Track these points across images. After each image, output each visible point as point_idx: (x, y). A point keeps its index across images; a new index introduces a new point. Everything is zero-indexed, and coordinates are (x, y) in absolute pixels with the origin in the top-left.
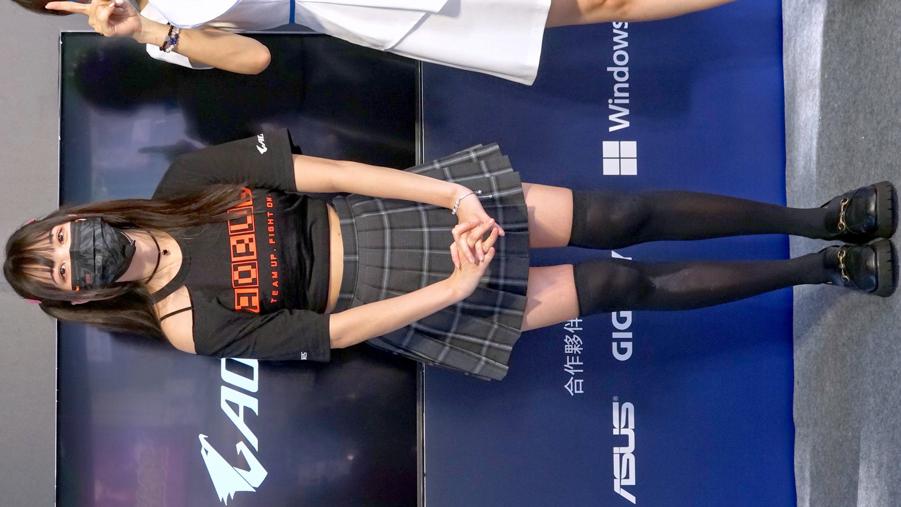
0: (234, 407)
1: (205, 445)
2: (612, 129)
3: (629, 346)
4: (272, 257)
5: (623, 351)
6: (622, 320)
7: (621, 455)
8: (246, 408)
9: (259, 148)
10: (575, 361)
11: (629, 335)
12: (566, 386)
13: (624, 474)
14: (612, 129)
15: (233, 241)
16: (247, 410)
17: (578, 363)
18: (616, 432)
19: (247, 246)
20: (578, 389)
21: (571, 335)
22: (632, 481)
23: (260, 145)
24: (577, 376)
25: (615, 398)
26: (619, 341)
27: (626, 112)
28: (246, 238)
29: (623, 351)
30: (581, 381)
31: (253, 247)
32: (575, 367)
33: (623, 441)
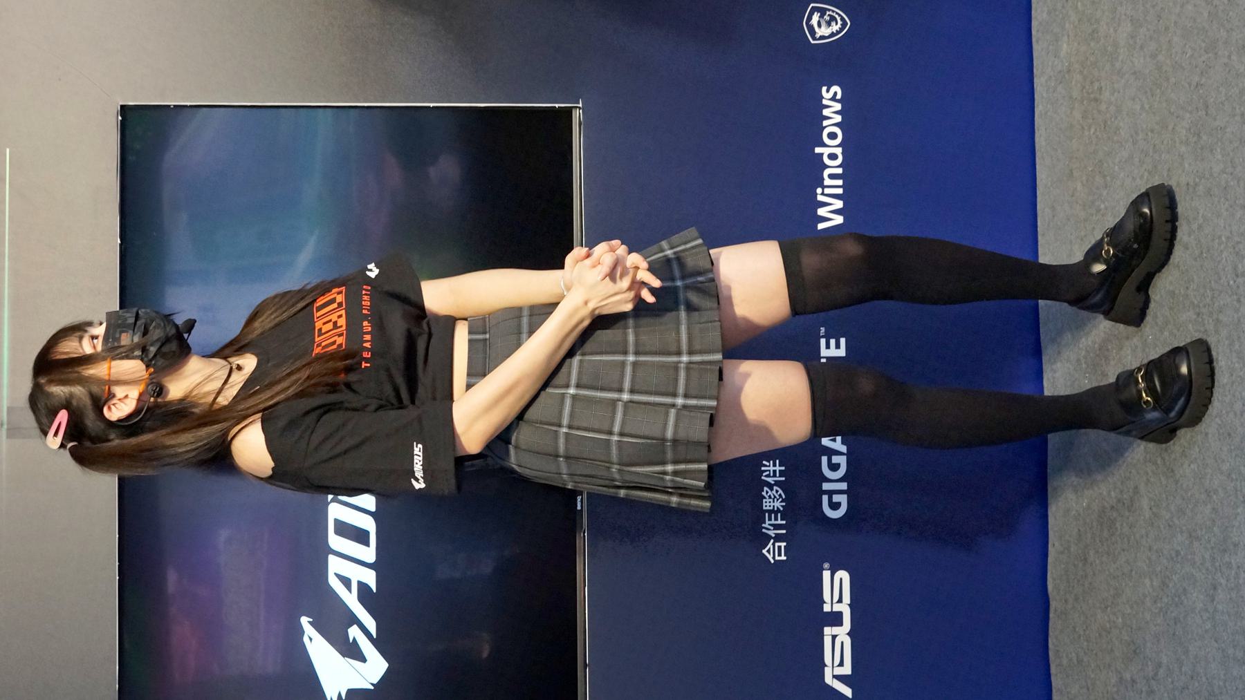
0: (346, 582)
1: (309, 630)
2: (821, 226)
3: (843, 499)
4: (365, 323)
5: (835, 506)
6: (834, 467)
7: (834, 637)
8: (360, 583)
9: (413, 482)
10: (776, 519)
11: (844, 486)
12: (764, 551)
13: (837, 661)
14: (821, 226)
15: (318, 325)
16: (363, 587)
17: (779, 522)
18: (827, 608)
19: (335, 323)
20: (780, 555)
21: (771, 486)
22: (847, 670)
23: (417, 480)
24: (778, 538)
25: (826, 565)
26: (831, 493)
27: (839, 204)
28: (334, 317)
29: (835, 506)
30: (783, 544)
31: (342, 322)
32: (776, 527)
33: (836, 619)
